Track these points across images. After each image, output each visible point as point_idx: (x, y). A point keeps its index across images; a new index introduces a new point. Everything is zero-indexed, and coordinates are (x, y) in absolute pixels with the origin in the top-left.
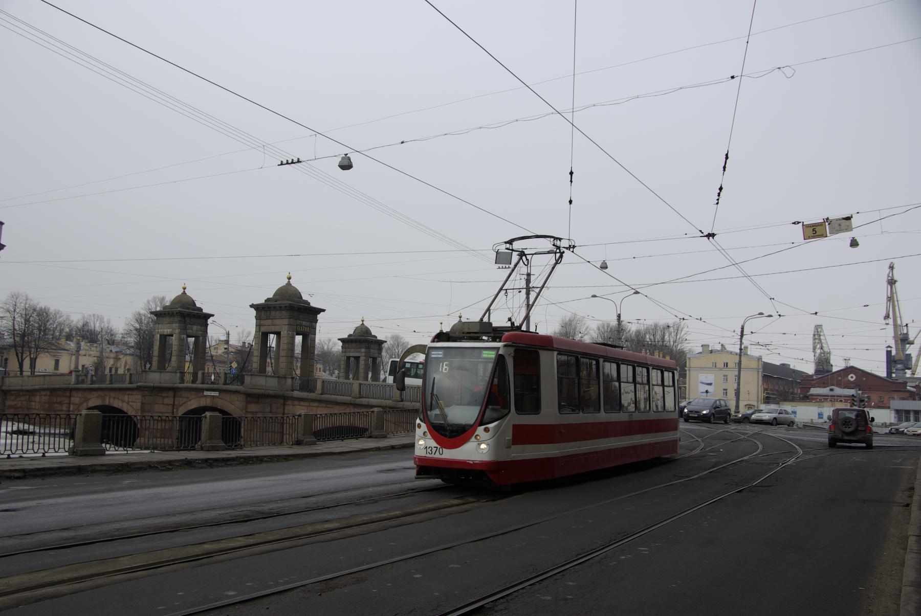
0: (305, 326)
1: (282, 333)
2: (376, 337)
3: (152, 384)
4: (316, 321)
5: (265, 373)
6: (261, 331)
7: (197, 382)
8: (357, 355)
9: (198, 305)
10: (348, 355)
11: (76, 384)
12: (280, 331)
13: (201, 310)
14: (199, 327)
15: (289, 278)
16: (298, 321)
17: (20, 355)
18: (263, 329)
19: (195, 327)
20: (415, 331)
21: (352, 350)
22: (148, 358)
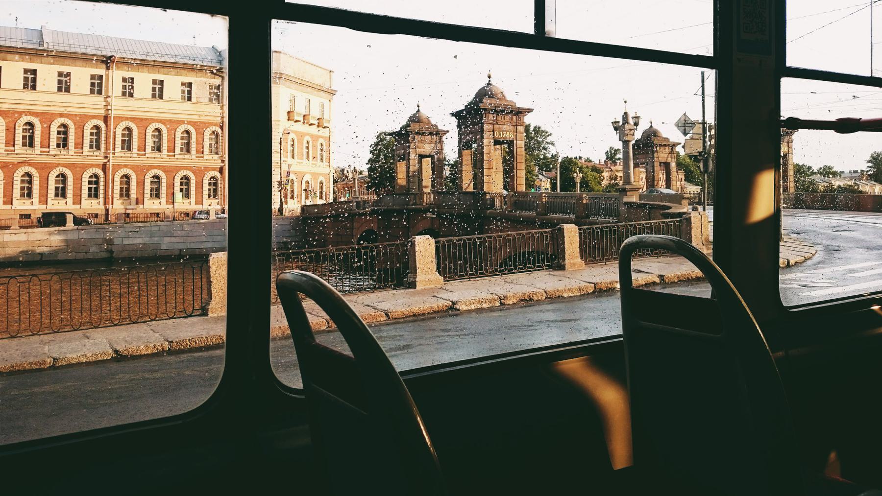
16: (495, 125)
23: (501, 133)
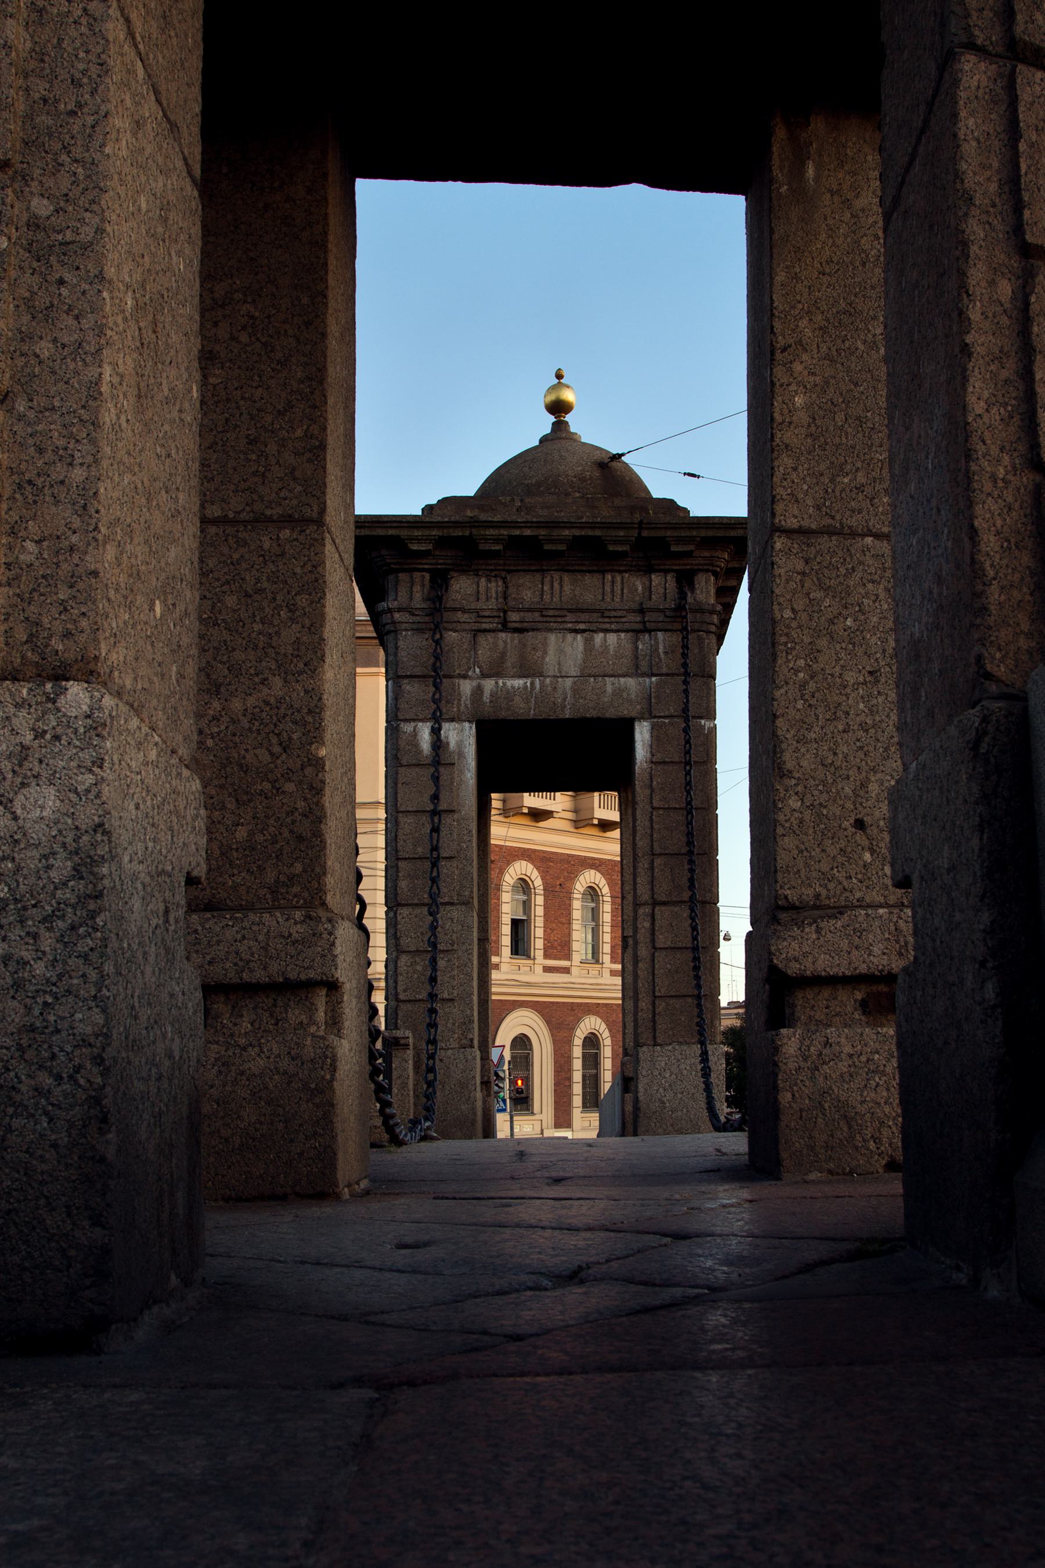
15: (558, 408)
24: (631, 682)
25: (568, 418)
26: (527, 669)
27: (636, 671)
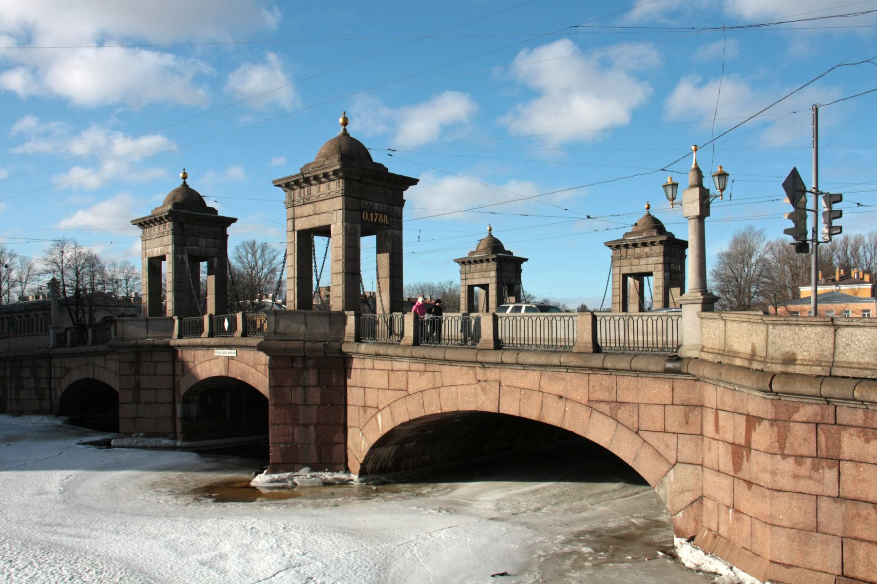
0: (379, 213)
1: (332, 227)
2: (512, 254)
3: (134, 342)
4: (401, 203)
5: (311, 309)
6: (297, 228)
7: (203, 335)
8: (483, 281)
9: (209, 204)
10: (470, 282)
11: (56, 348)
12: (327, 223)
13: (213, 211)
14: (211, 240)
16: (363, 201)
17: (74, 316)
18: (303, 224)
19: (203, 242)
20: (589, 217)
21: (476, 275)
22: (677, 372)
23: (372, 214)
24: (213, 249)
25: (186, 180)
26: (197, 245)
27: (215, 247)
